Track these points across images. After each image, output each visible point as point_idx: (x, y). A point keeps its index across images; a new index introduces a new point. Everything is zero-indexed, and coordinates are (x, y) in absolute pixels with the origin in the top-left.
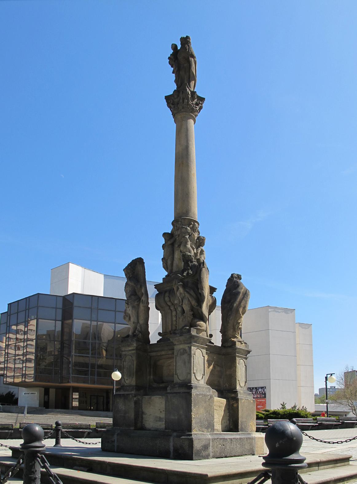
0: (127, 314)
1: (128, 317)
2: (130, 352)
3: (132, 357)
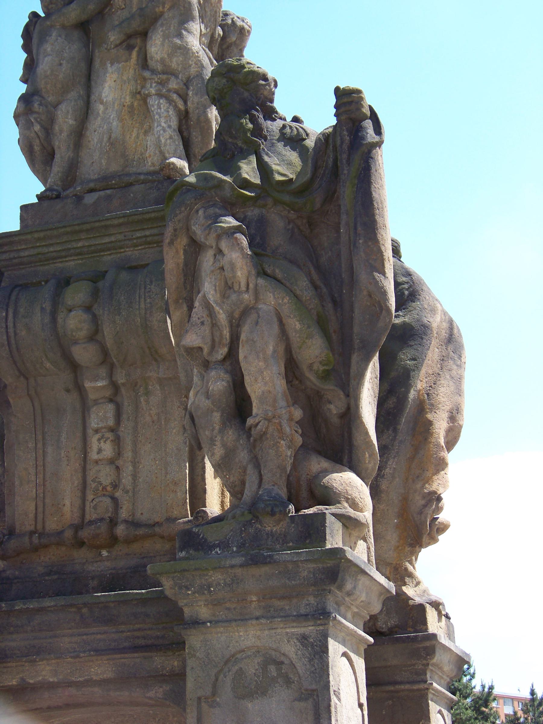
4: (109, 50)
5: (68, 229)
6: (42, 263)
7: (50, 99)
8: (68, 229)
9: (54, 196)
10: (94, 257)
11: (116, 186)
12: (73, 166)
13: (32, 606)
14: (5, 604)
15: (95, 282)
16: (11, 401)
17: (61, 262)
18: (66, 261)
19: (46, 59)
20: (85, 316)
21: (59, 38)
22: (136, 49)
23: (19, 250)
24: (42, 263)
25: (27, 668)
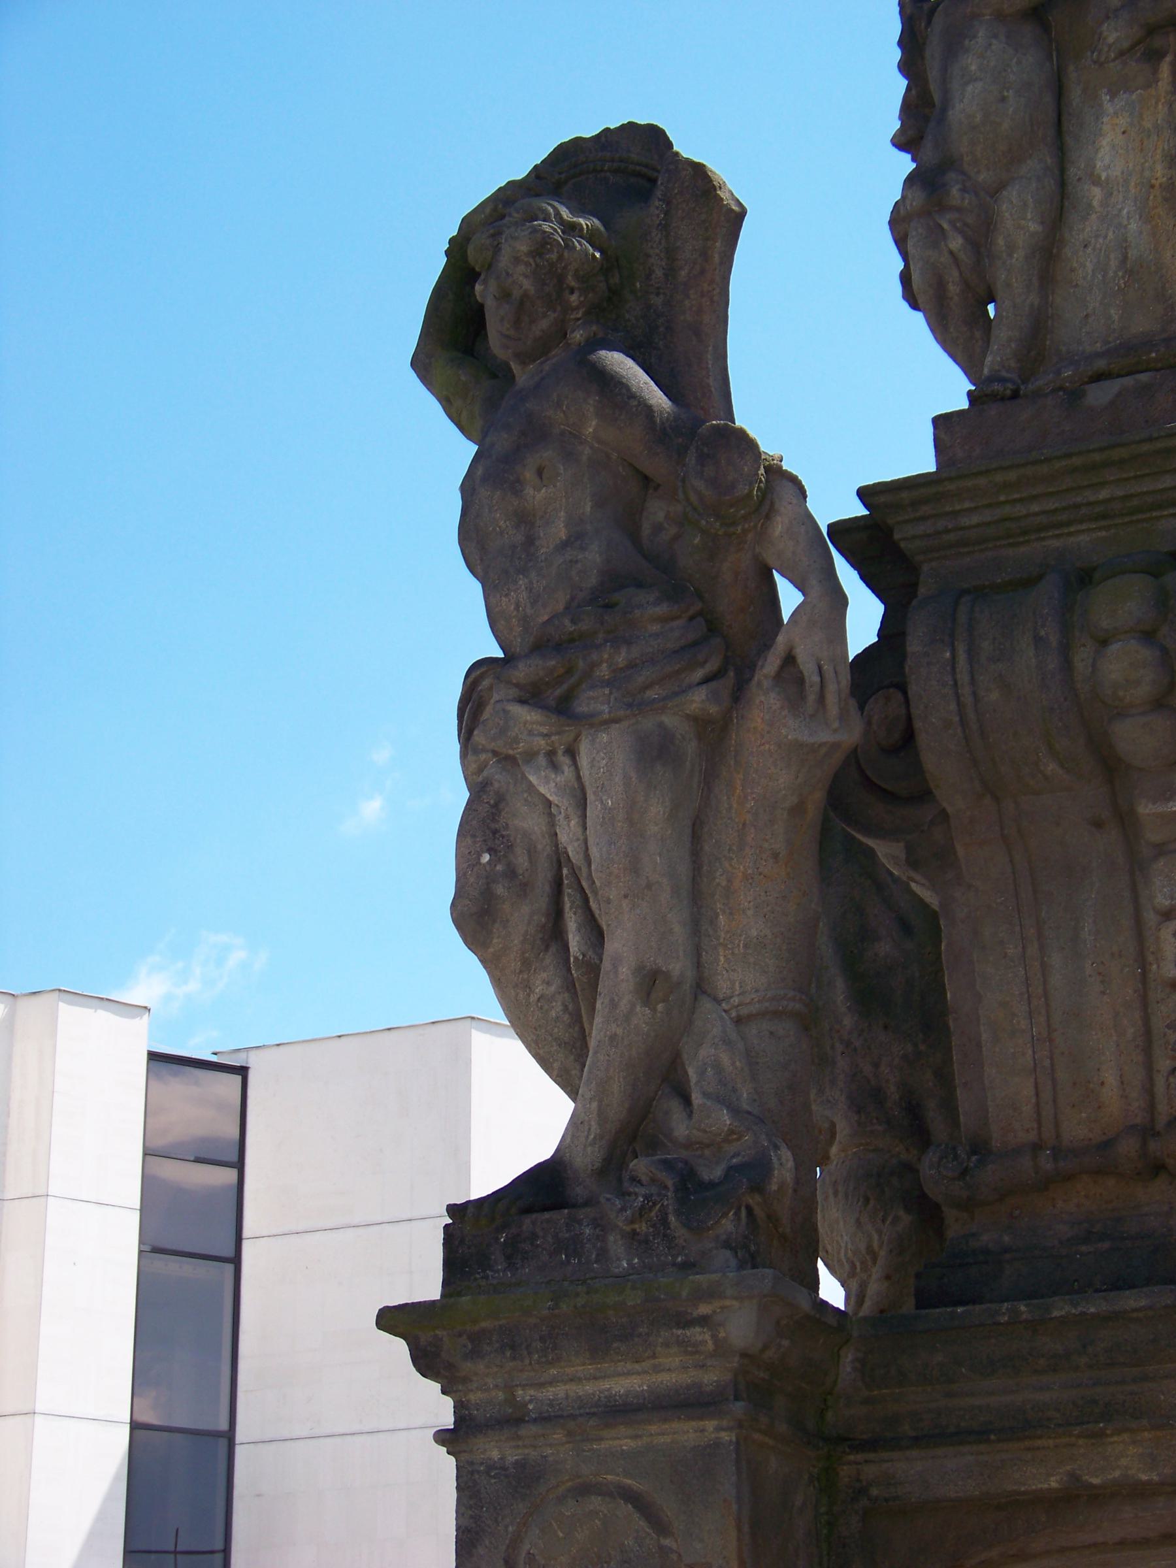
0: (521, 860)
1: (540, 900)
2: (621, 1440)
3: (661, 1527)
4: (1101, 64)
5: (1077, 461)
6: (1011, 541)
7: (981, 178)
8: (1077, 461)
9: (1008, 392)
10: (1138, 521)
11: (1160, 365)
12: (1039, 326)
13: (1092, 1310)
14: (1026, 1306)
15: (1156, 575)
16: (960, 851)
17: (1058, 536)
18: (1070, 534)
19: (970, 88)
20: (1146, 653)
21: (994, 41)
22: (1168, 58)
23: (955, 514)
24: (1011, 541)
25: (1082, 1451)
